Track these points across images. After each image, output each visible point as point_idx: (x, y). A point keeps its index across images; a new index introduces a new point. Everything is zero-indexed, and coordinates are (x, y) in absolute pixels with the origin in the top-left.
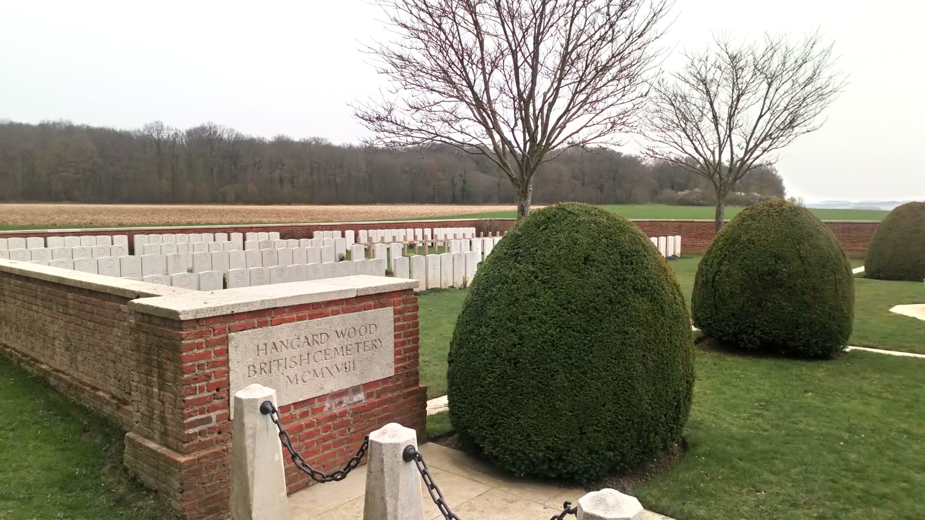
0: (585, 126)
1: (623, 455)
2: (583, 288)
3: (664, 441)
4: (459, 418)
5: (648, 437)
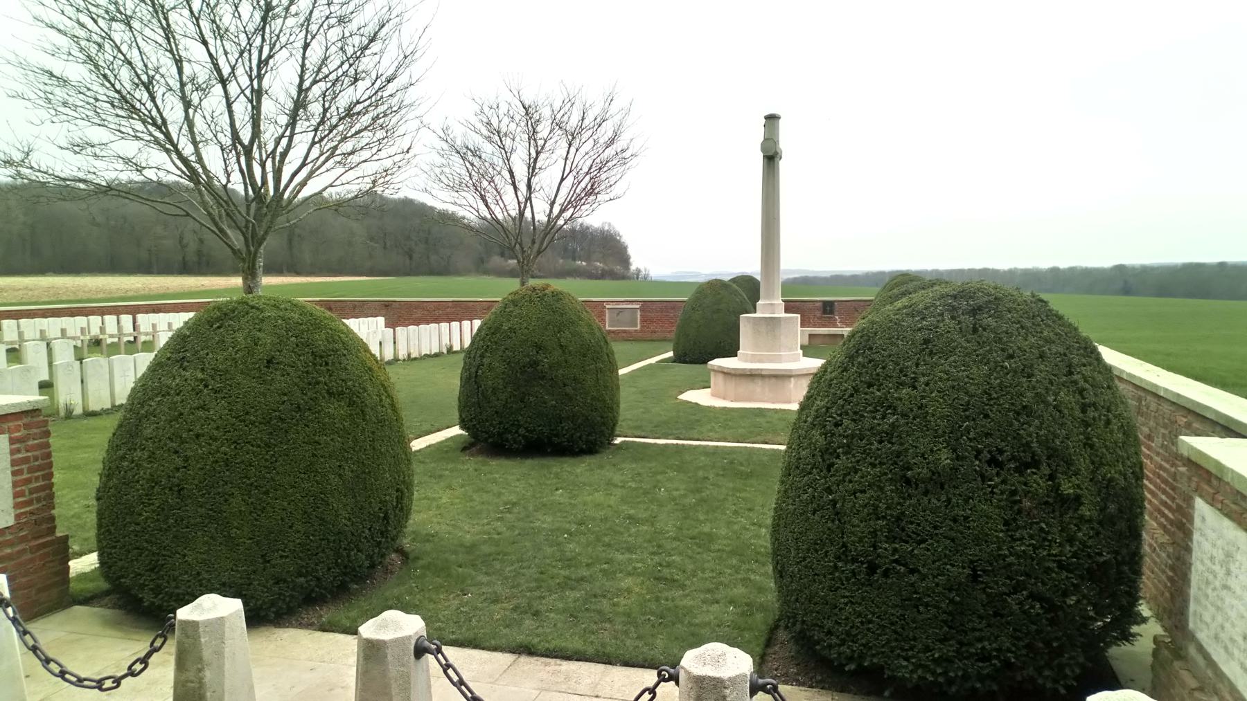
0: (331, 185)
1: (318, 579)
2: (264, 395)
3: (370, 557)
4: (110, 567)
5: (349, 556)
